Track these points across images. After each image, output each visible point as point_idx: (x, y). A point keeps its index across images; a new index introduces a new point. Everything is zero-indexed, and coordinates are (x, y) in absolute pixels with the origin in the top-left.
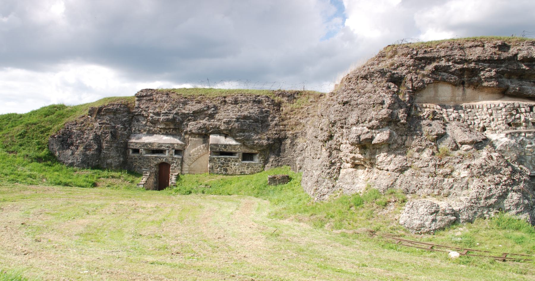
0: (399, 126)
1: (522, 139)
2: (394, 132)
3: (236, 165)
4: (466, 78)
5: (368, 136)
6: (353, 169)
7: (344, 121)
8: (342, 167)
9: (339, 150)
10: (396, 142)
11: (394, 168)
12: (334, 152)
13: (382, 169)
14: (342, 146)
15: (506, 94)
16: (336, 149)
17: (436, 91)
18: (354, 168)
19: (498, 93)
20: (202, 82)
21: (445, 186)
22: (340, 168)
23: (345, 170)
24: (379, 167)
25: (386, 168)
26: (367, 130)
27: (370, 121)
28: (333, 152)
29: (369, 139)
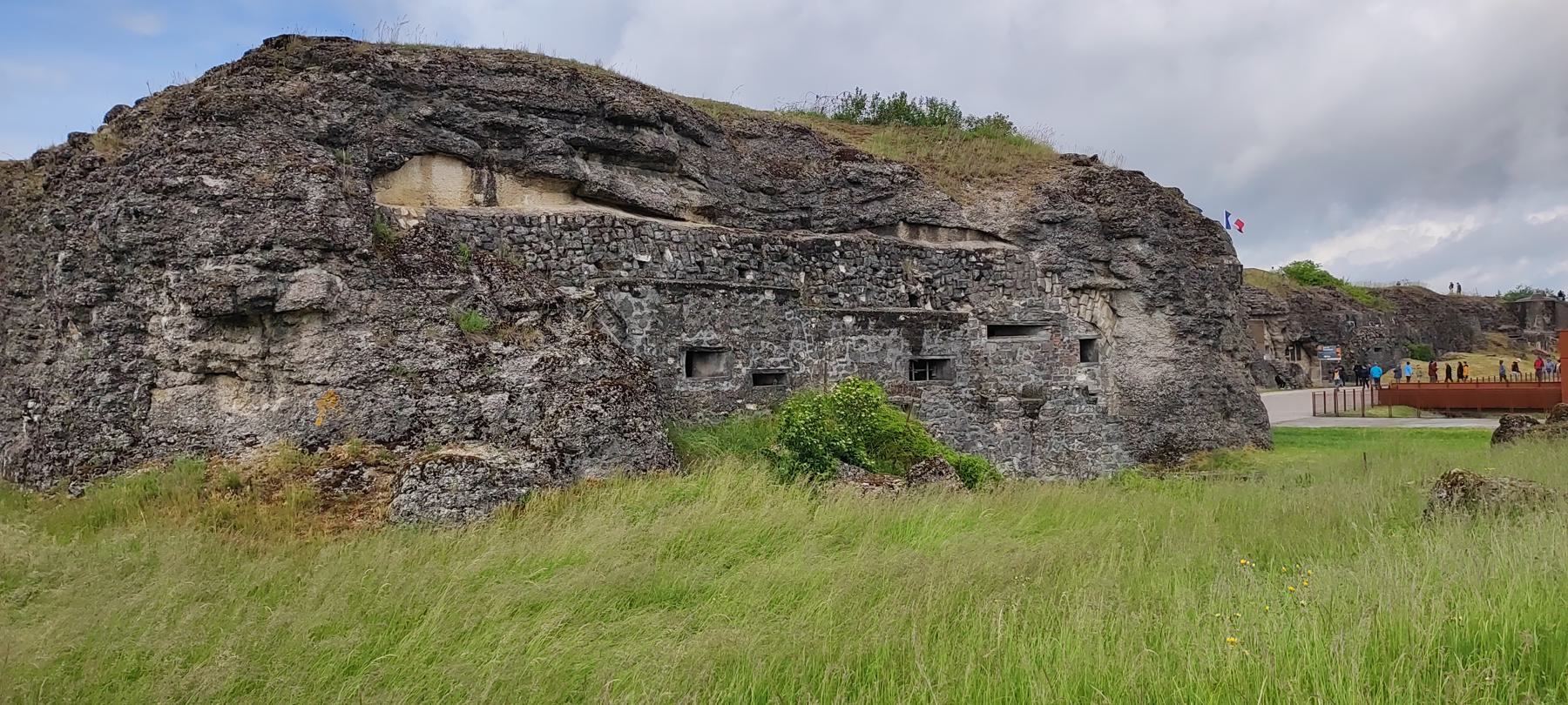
0: (351, 263)
1: (626, 298)
2: (338, 280)
3: (541, 500)
4: (498, 148)
5: (264, 288)
6: (199, 388)
7: (168, 245)
8: (159, 382)
9: (145, 331)
10: (344, 304)
11: (346, 378)
12: (127, 341)
13: (304, 381)
14: (154, 320)
15: (578, 193)
16: (131, 329)
17: (427, 176)
18: (201, 382)
19: (564, 192)
20: (1270, 396)
21: (489, 413)
22: (153, 386)
23: (170, 391)
24: (294, 377)
25: (319, 379)
26: (254, 274)
27: (267, 247)
28: (122, 341)
29: (266, 298)
